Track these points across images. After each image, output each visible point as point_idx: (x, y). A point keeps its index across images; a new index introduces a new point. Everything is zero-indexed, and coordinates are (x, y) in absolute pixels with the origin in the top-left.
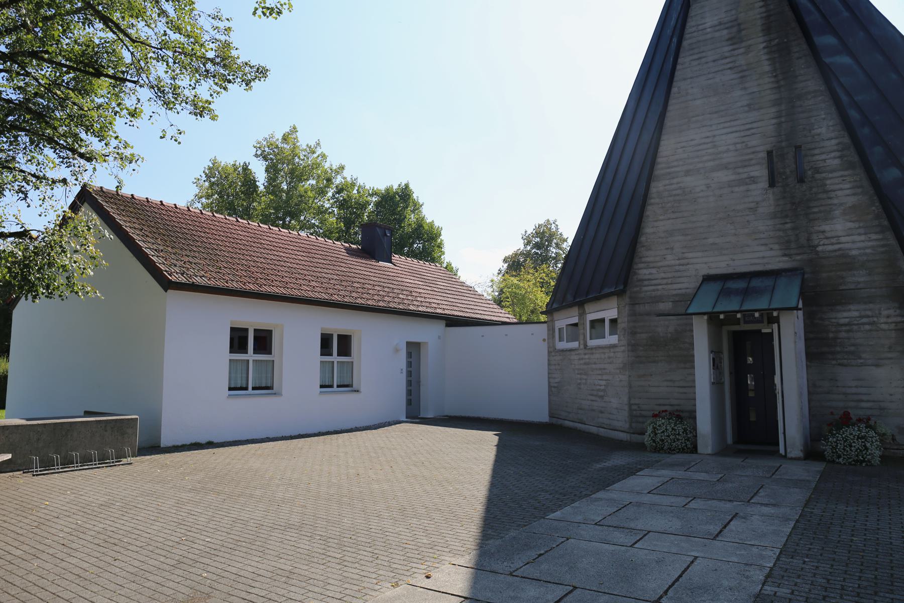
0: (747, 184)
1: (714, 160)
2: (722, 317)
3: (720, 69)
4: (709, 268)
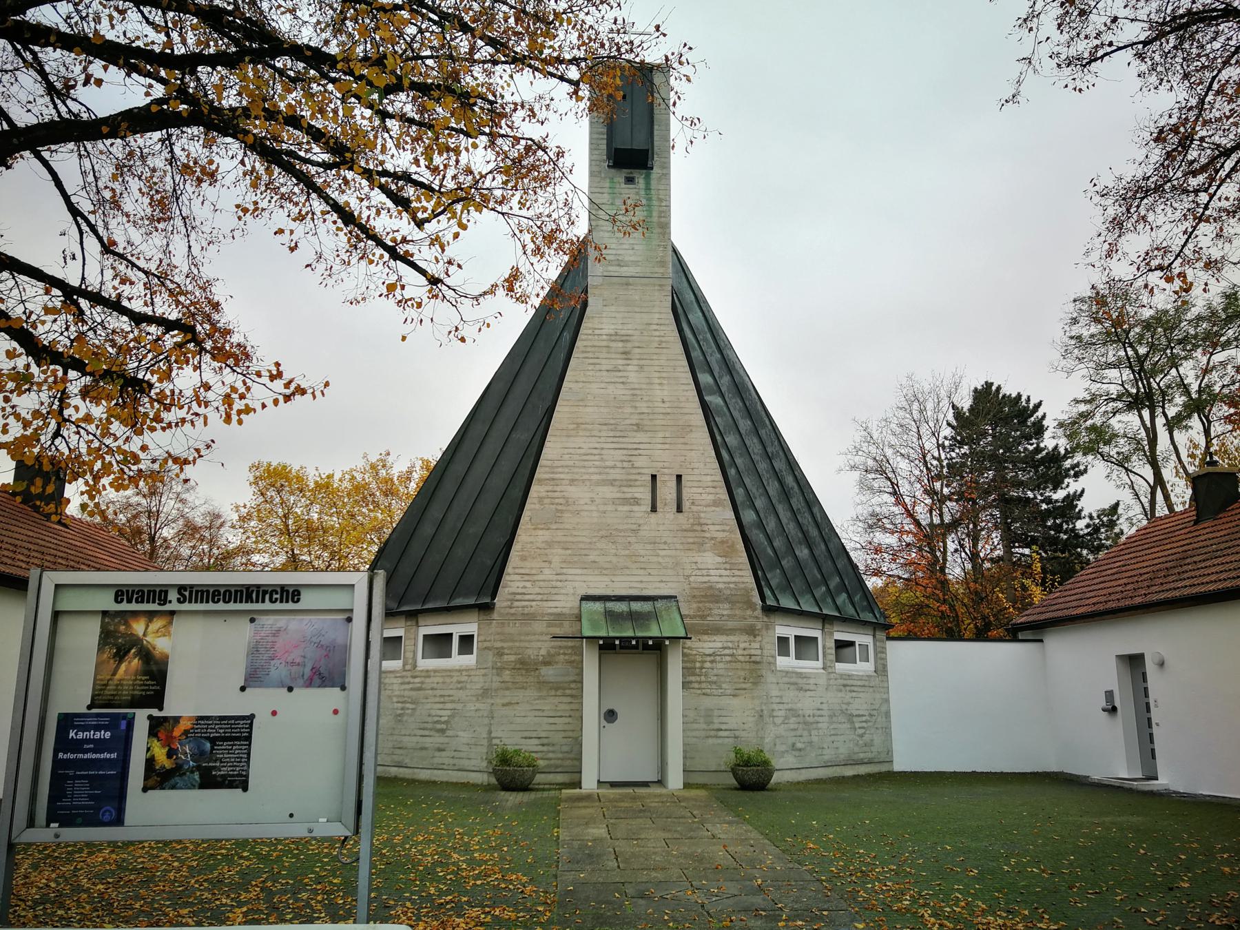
1: (600, 473)
2: (617, 642)
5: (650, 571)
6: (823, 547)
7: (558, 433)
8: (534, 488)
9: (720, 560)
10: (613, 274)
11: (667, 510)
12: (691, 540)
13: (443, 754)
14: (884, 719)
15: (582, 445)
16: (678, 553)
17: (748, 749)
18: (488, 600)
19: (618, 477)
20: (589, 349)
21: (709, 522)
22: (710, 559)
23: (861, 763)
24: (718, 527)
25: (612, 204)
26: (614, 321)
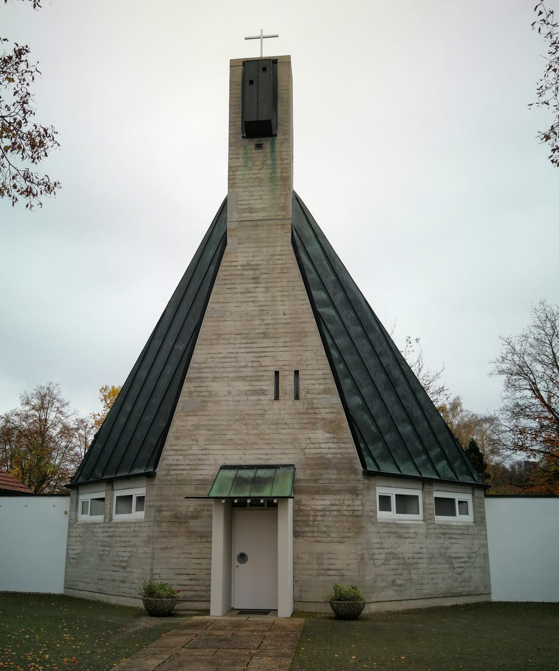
0: (259, 395)
1: (235, 372)
2: (249, 501)
3: (246, 300)
4: (226, 459)
5: (273, 446)
6: (425, 423)
7: (204, 342)
8: (185, 385)
9: (328, 435)
10: (246, 219)
11: (287, 400)
12: (306, 421)
13: (124, 585)
14: (482, 560)
15: (222, 351)
16: (296, 431)
17: (345, 587)
18: (151, 470)
19: (249, 374)
20: (227, 277)
21: (320, 406)
22: (320, 435)
23: (460, 595)
24: (327, 410)
25: (245, 166)
26: (246, 255)
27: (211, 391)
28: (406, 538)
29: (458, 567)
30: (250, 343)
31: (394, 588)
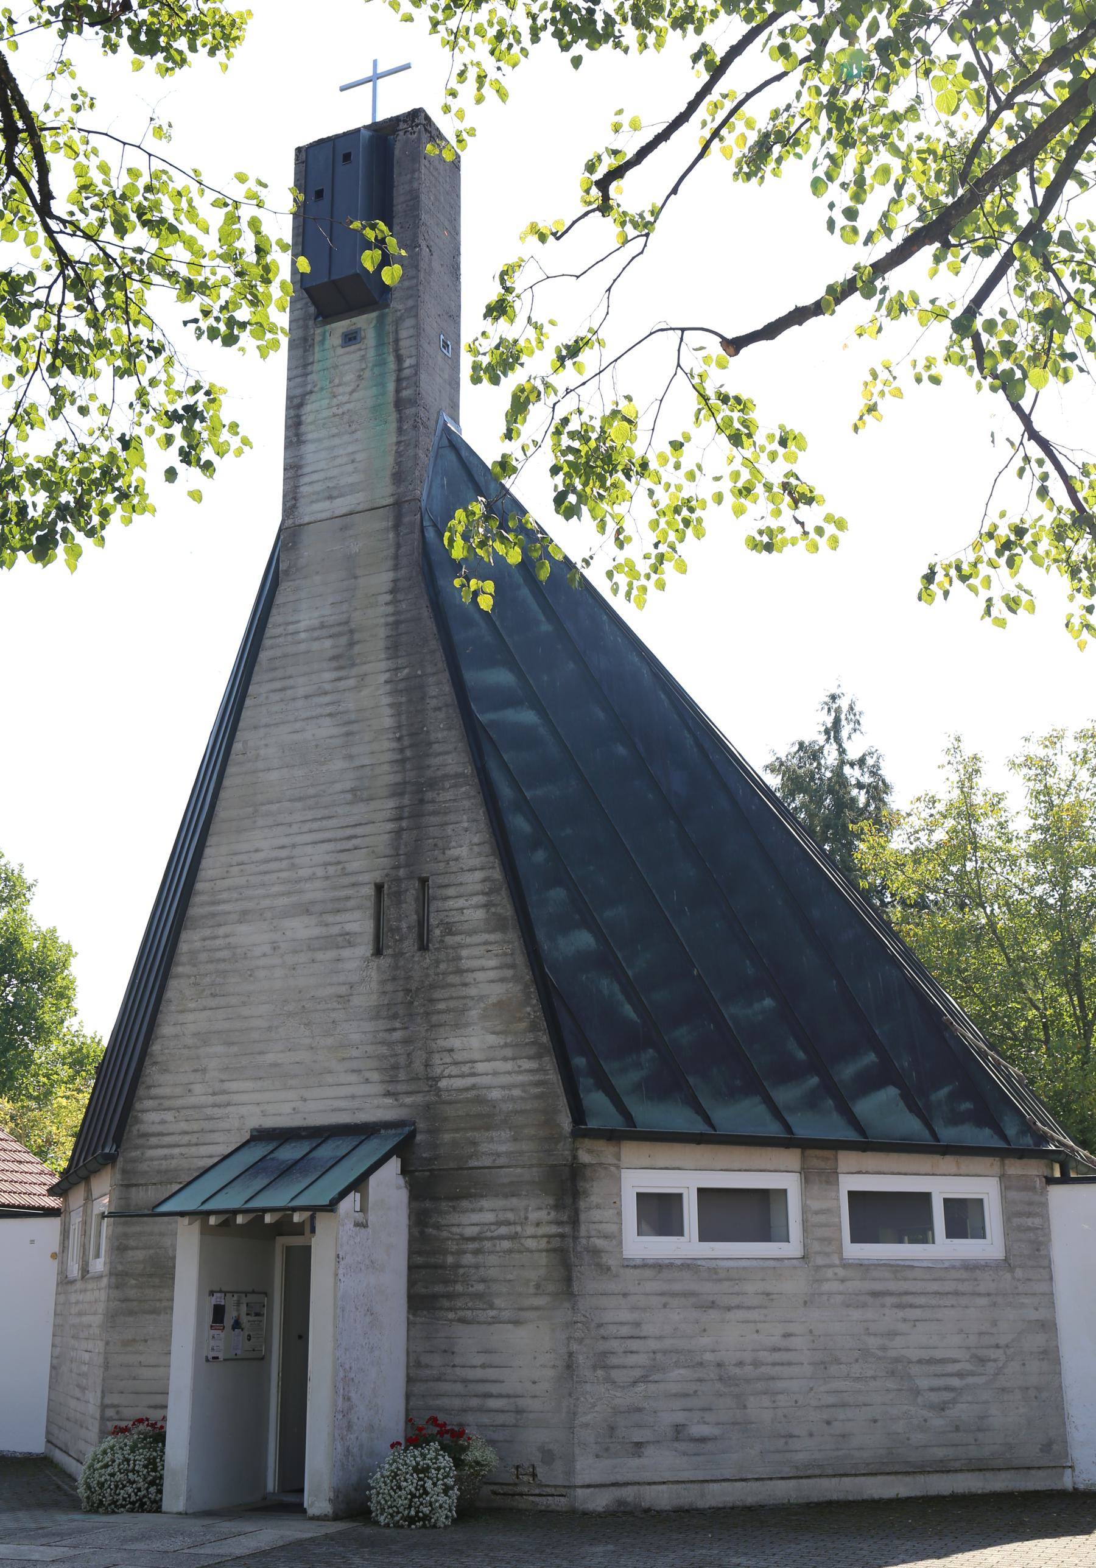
1: (289, 893)
3: (314, 714)
4: (264, 1114)
9: (492, 1039)
19: (319, 895)
27: (235, 948)
28: (729, 1309)
29: (932, 1389)
30: (323, 818)
31: (682, 1446)
